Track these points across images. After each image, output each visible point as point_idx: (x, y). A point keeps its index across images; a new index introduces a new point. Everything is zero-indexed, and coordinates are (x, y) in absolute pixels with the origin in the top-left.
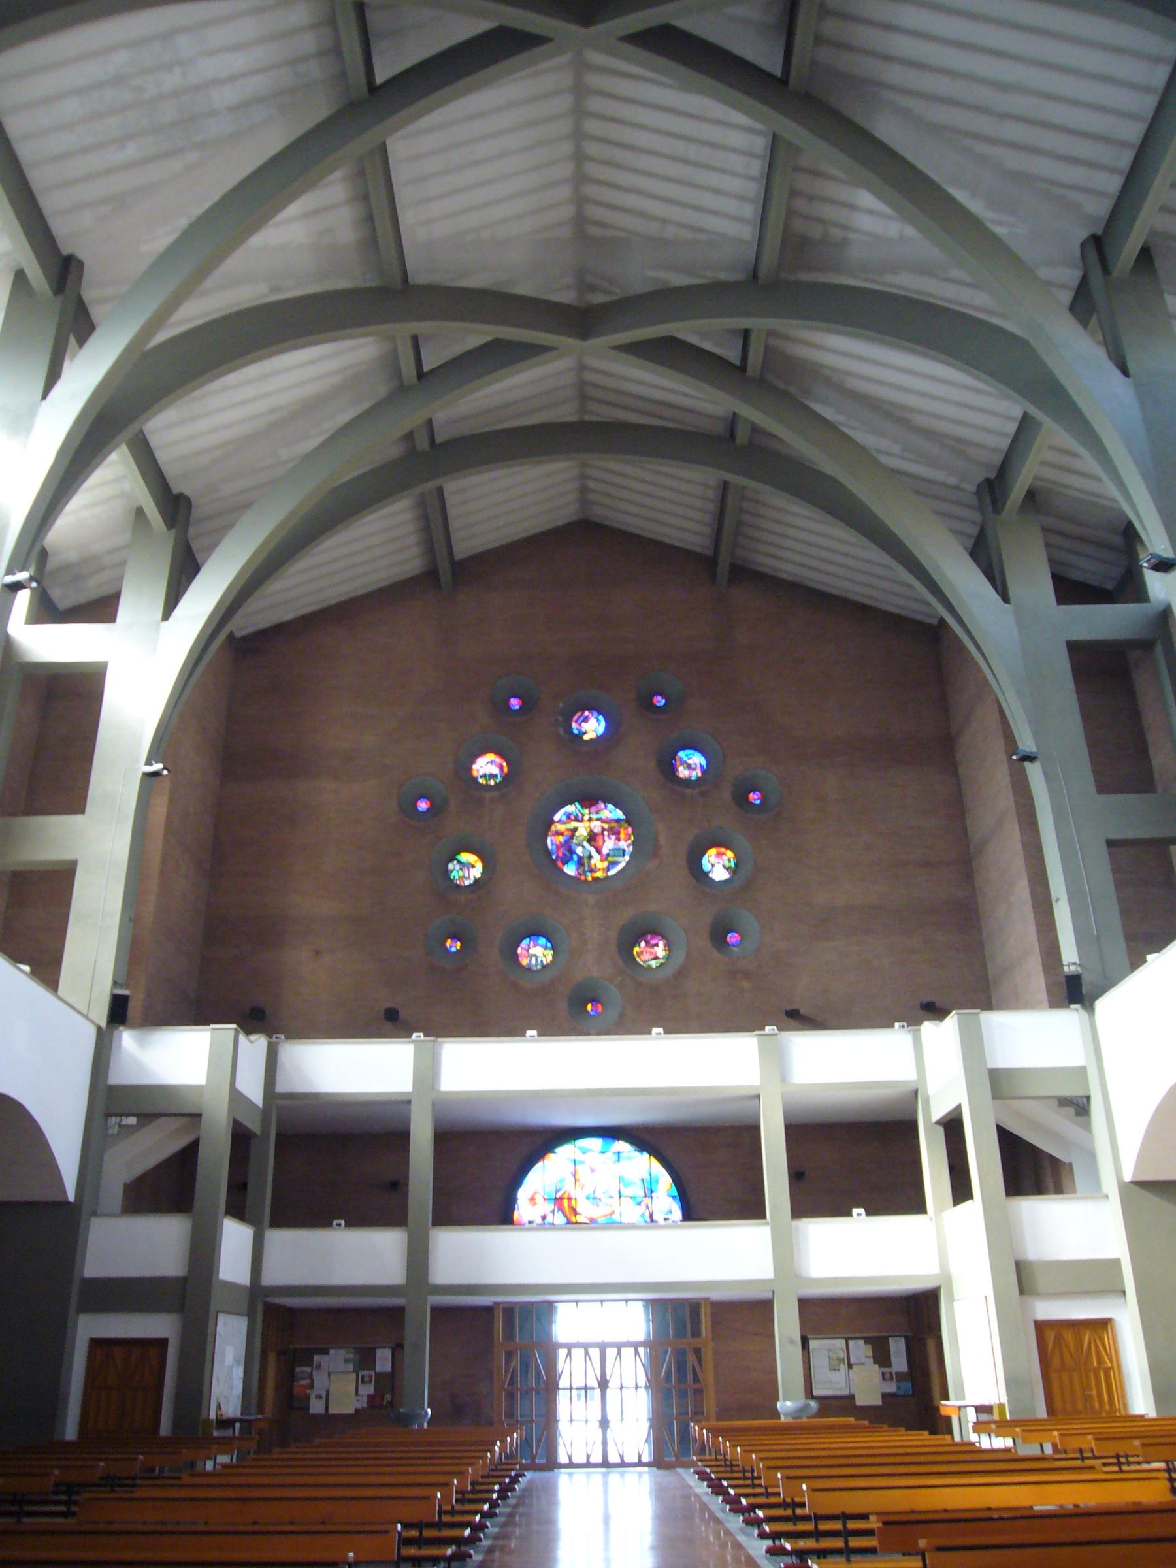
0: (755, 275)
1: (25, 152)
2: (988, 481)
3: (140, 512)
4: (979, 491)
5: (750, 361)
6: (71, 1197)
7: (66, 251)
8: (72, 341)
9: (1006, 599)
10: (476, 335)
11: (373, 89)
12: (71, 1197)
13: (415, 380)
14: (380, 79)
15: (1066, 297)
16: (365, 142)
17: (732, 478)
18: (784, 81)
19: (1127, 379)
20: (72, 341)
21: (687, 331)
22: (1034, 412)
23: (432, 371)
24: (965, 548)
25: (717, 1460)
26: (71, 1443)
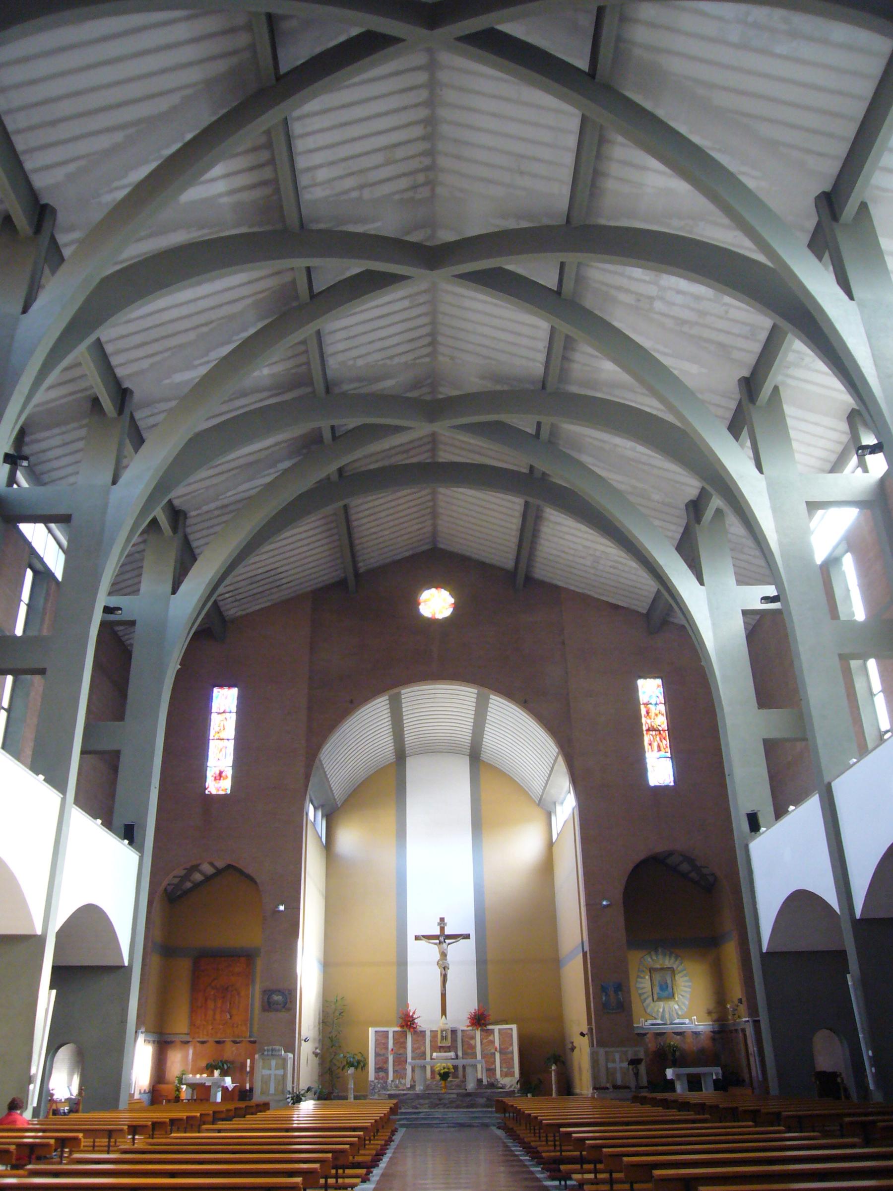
0: (544, 387)
1: (20, 143)
2: (824, 193)
3: (95, 402)
4: (687, 505)
5: (542, 432)
6: (126, 964)
7: (125, 386)
8: (47, 271)
9: (851, 298)
10: (355, 267)
11: (278, 78)
12: (126, 964)
13: (274, 82)
14: (283, 70)
15: (806, 238)
16: (270, 119)
17: (530, 500)
18: (559, 293)
19: (852, 302)
20: (47, 271)
21: (516, 265)
22: (708, 487)
23: (341, 436)
24: (673, 546)
25: (540, 1141)
26: (219, 1103)
